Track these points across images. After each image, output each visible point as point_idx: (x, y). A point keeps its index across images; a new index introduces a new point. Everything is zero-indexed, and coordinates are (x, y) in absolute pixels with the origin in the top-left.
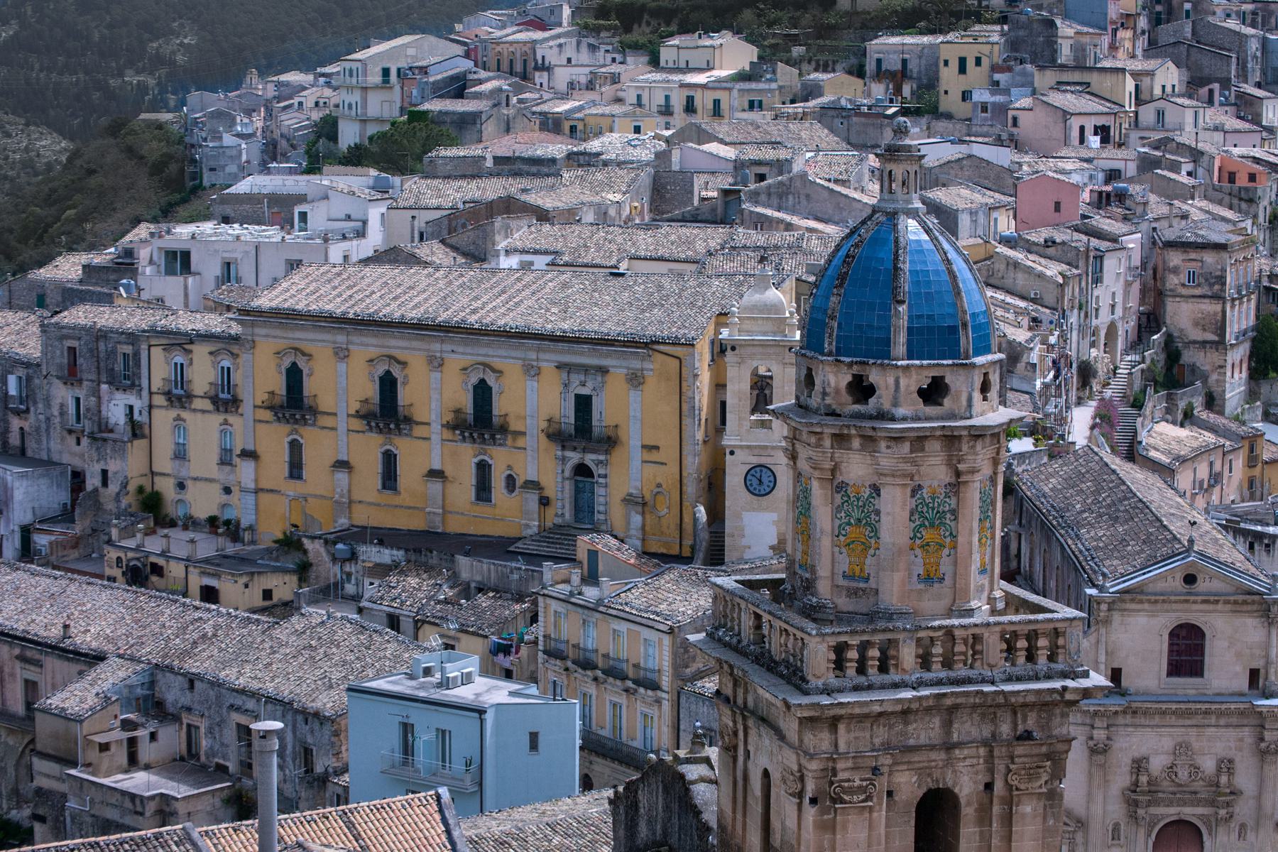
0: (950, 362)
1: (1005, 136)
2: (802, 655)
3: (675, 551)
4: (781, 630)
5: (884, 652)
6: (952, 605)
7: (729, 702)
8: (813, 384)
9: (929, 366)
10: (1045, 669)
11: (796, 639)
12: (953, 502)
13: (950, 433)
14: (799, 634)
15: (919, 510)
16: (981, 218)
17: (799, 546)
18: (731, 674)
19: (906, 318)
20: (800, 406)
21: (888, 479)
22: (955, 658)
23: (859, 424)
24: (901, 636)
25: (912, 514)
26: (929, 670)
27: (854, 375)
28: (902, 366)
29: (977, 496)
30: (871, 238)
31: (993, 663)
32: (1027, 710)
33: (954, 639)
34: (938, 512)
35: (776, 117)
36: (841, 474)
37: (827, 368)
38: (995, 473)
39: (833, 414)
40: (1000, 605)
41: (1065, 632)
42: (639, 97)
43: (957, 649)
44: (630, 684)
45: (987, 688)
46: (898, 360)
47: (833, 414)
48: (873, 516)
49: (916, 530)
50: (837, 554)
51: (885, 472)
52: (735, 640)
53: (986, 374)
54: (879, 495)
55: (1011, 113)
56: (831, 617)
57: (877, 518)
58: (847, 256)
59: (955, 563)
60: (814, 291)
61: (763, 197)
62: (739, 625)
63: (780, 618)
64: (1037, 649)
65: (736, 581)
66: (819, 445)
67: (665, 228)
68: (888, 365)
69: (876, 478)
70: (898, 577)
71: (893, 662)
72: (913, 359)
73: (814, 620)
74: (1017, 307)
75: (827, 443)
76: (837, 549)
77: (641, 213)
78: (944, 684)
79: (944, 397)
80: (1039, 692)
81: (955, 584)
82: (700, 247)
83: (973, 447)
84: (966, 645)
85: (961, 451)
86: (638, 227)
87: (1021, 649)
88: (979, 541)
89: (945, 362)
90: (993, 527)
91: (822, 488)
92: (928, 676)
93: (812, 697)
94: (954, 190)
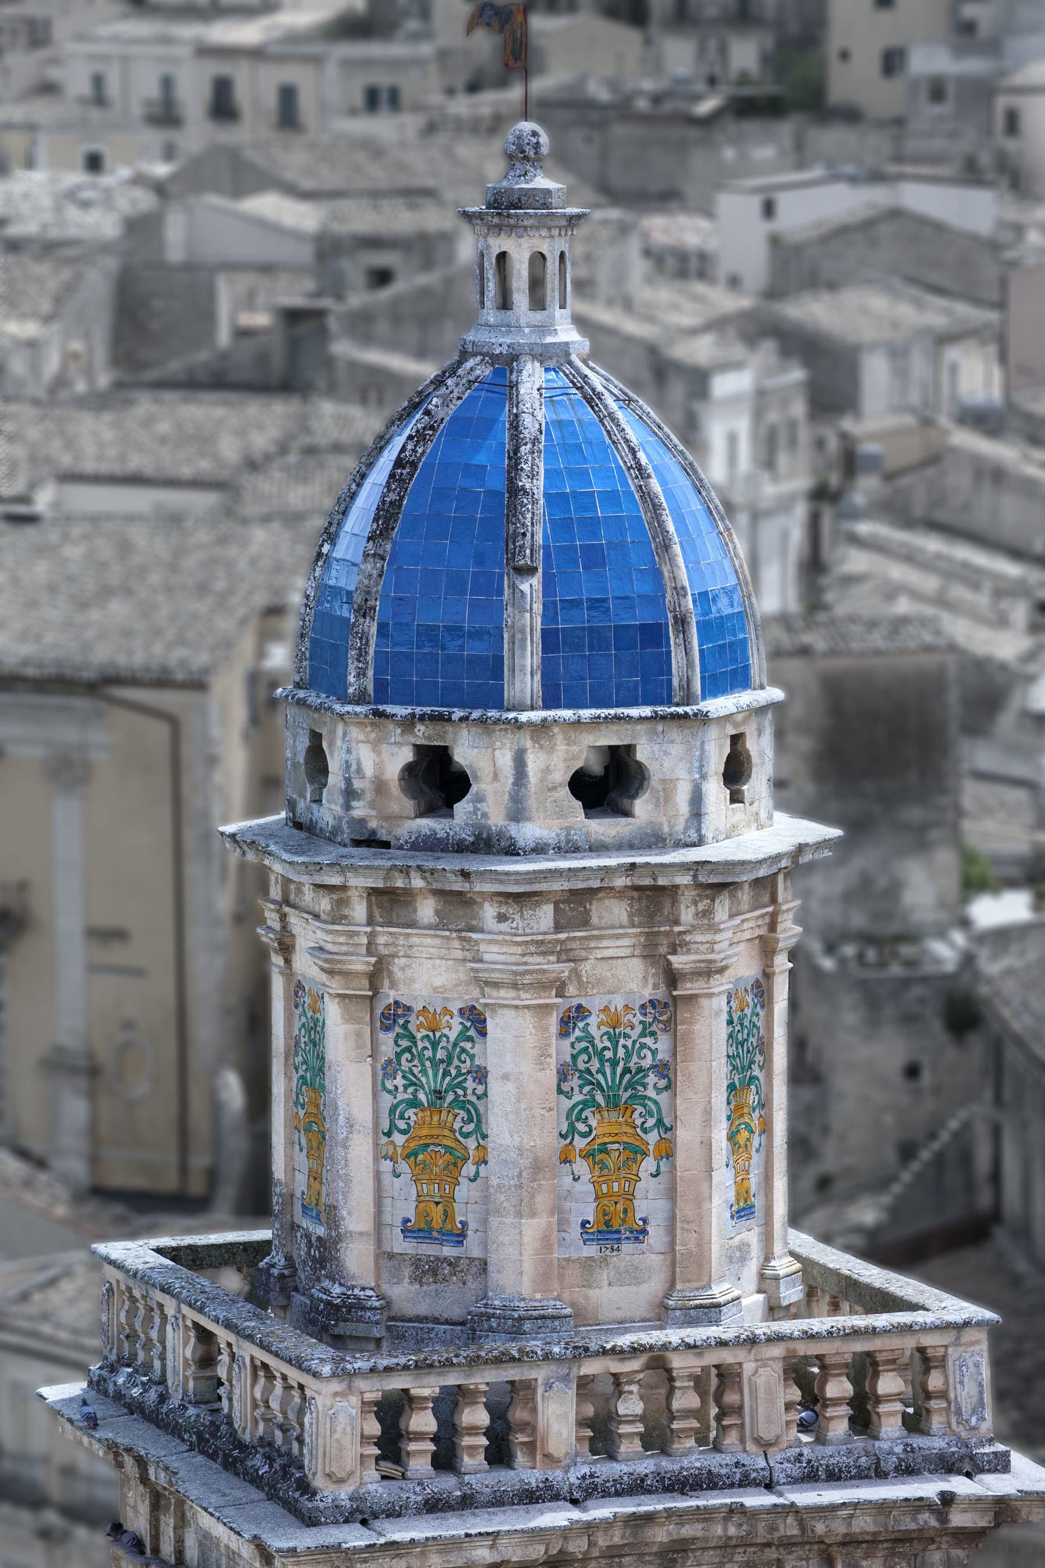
0: (646, 711)
1: (985, 159)
2: (302, 1425)
3: (169, 1182)
4: (254, 1368)
5: (498, 1413)
6: (668, 1295)
7: (142, 1553)
8: (324, 771)
9: (596, 721)
10: (898, 1449)
11: (288, 1388)
12: (662, 1045)
13: (647, 882)
14: (295, 1376)
15: (581, 1066)
16: (919, 365)
17: (301, 1160)
18: (144, 1480)
19: (538, 608)
20: (298, 826)
21: (503, 993)
22: (675, 1426)
23: (430, 865)
24: (540, 1374)
25: (563, 1076)
26: (612, 1457)
27: (418, 749)
28: (530, 724)
29: (722, 1030)
30: (455, 419)
31: (767, 1433)
32: (859, 1553)
33: (671, 1379)
34: (627, 1070)
35: (431, 129)
36: (393, 985)
37: (355, 733)
38: (767, 976)
39: (371, 842)
40: (792, 1293)
41: (944, 1358)
42: (98, 82)
43: (679, 1403)
44: (51, 1518)
45: (756, 1500)
46: (522, 709)
47: (371, 842)
48: (470, 1084)
49: (575, 1115)
50: (387, 1179)
51: (496, 976)
52: (153, 1395)
53: (736, 740)
54: (483, 1033)
55: (1002, 103)
56: (377, 1332)
57: (480, 1089)
58: (399, 463)
59: (671, 1194)
60: (326, 549)
61: (382, 327)
62: (163, 1358)
63: (250, 1338)
64: (878, 1400)
65: (159, 1251)
66: (338, 917)
67: (144, 405)
68: (498, 721)
69: (476, 992)
70: (533, 1228)
71: (522, 1438)
72: (558, 706)
73: (338, 1341)
74: (996, 576)
75: (359, 910)
76: (387, 1165)
77: (89, 372)
78: (649, 1492)
79: (634, 797)
80: (883, 1507)
81: (672, 1244)
82: (229, 449)
83: (707, 913)
84: (703, 1394)
85: (677, 922)
86: (81, 403)
87: (836, 1402)
88: (731, 1137)
89: (634, 712)
90: (765, 1104)
91: (349, 1018)
92: (607, 1470)
93: (324, 1530)
94: (852, 297)
